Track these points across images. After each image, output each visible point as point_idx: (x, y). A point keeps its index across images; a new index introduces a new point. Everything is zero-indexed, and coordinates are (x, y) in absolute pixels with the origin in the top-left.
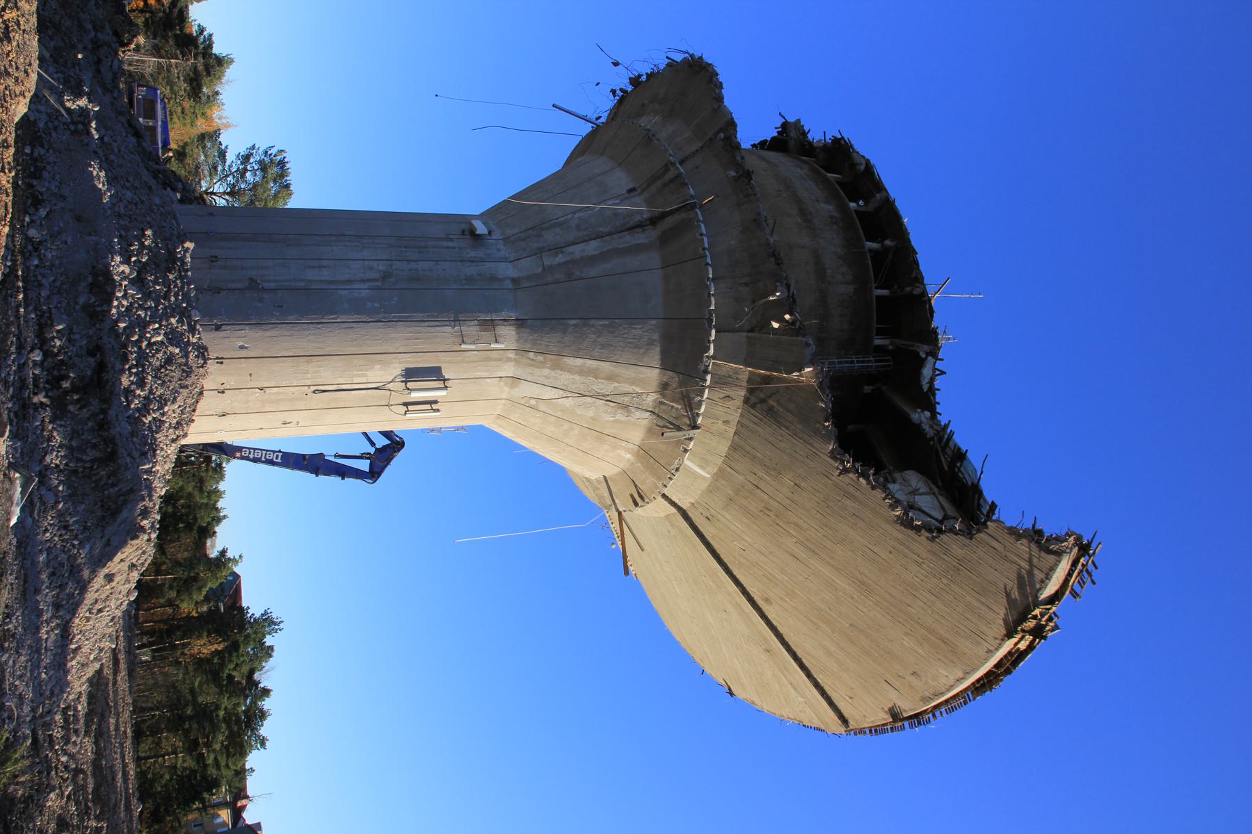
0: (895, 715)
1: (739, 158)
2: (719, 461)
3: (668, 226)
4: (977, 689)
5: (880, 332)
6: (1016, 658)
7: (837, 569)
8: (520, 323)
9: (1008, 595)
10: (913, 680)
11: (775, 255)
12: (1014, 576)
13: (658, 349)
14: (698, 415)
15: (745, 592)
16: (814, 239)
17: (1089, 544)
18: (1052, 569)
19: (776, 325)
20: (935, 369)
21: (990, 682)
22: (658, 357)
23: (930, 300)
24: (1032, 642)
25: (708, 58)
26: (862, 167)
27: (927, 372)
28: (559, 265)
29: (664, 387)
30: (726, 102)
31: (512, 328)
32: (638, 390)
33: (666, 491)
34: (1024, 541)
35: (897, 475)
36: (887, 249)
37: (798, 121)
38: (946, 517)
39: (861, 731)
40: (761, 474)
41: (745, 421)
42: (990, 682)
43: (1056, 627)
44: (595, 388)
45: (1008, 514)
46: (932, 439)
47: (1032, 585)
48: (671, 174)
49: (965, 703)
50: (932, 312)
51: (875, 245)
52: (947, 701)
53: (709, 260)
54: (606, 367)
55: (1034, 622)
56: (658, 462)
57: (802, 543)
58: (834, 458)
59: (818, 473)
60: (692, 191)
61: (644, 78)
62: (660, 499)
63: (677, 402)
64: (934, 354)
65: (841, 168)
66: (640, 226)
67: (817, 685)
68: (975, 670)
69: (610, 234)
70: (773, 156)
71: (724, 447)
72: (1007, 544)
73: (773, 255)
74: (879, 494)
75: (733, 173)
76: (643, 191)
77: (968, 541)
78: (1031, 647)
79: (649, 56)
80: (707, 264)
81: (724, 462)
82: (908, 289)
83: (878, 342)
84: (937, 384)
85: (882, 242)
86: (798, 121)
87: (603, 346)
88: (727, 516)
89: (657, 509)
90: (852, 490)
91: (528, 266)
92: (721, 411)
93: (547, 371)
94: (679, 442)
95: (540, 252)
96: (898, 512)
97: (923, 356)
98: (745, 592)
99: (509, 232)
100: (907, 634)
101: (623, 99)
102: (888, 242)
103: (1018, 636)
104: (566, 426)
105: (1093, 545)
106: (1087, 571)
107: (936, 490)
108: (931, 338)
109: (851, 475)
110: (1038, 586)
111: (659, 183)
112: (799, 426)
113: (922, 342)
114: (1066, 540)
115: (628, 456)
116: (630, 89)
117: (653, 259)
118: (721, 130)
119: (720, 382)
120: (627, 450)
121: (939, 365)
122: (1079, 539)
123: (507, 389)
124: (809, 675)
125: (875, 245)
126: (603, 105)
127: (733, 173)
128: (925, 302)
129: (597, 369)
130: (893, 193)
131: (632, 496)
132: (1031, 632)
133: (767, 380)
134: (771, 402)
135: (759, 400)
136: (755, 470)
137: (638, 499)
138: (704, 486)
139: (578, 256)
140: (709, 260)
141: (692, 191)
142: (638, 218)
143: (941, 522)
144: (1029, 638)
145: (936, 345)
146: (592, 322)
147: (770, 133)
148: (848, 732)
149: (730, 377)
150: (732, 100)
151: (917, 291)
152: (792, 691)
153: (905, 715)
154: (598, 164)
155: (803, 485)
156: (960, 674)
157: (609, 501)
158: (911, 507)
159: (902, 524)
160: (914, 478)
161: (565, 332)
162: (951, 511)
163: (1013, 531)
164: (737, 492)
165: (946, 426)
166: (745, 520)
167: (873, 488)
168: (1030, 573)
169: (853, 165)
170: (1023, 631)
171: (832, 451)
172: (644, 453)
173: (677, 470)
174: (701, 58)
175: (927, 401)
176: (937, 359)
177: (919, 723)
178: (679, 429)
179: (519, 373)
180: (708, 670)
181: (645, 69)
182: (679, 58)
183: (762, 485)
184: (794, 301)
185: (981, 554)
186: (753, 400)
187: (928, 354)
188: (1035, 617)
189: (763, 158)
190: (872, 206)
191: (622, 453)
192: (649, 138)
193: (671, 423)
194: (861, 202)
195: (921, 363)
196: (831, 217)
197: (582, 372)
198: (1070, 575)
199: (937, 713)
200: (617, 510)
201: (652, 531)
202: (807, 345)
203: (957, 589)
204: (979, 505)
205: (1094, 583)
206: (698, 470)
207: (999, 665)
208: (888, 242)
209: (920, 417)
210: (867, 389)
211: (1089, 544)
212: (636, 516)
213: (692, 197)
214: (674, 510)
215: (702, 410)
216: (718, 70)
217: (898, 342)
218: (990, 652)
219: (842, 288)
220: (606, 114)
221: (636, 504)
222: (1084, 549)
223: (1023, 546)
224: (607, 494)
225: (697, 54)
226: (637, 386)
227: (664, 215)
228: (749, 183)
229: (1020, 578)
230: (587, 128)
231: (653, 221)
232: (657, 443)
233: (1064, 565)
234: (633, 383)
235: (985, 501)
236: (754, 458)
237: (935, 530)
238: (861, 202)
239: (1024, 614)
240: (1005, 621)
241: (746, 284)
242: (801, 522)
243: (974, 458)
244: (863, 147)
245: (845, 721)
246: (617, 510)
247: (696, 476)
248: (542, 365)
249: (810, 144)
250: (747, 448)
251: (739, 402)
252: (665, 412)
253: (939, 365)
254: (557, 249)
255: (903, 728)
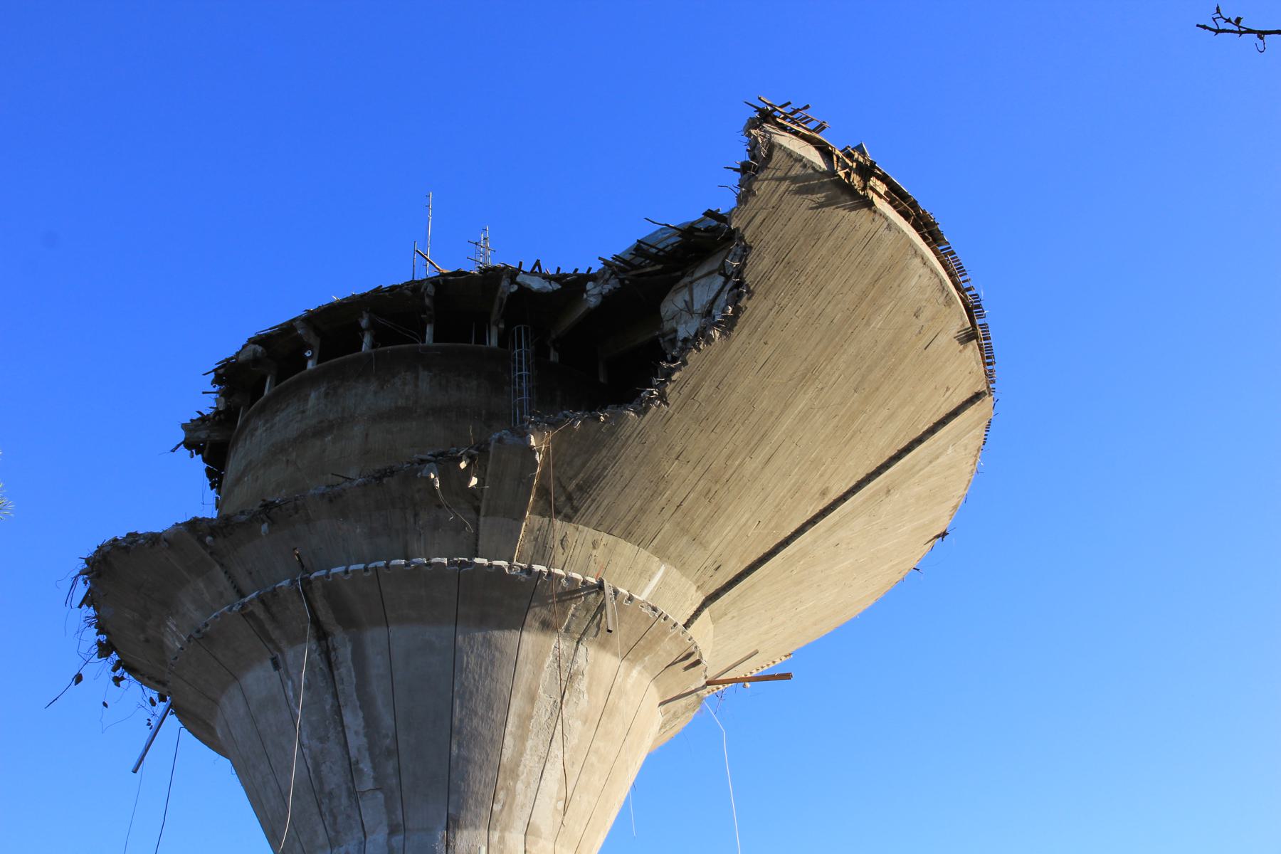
0: (968, 337)
1: (243, 518)
2: (644, 554)
3: (332, 617)
4: (935, 240)
5: (481, 339)
6: (897, 196)
7: (786, 406)
8: (453, 824)
9: (821, 205)
10: (923, 316)
11: (380, 476)
12: (798, 199)
13: (497, 633)
14: (584, 582)
15: (813, 521)
16: (361, 422)
17: (758, 110)
18: (790, 154)
19: (474, 481)
20: (532, 273)
21: (926, 225)
22: (507, 633)
23: (443, 275)
24: (878, 177)
25: (90, 549)
26: (259, 349)
27: (536, 284)
28: (374, 768)
29: (546, 626)
30: (157, 528)
31: (458, 836)
32: (550, 659)
33: (681, 624)
34: (755, 186)
35: (667, 326)
36: (373, 325)
37: (184, 426)
38: (722, 271)
39: (989, 375)
40: (663, 501)
41: (594, 521)
42: (926, 225)
43: (860, 149)
44: (544, 719)
45: (725, 203)
46: (622, 281)
47: (808, 178)
48: (260, 612)
49: (952, 253)
50: (458, 273)
51: (367, 340)
52: (951, 275)
53: (382, 564)
54: (517, 704)
55: (853, 176)
56: (645, 634)
57: (752, 451)
58: (646, 411)
59: (666, 432)
60: (285, 583)
61: (103, 638)
62: (690, 631)
63: (567, 609)
64: (513, 274)
65: (258, 378)
66: (327, 655)
67: (932, 430)
68: (911, 244)
69: (335, 696)
70: (234, 465)
71: (627, 548)
72: (758, 206)
73: (380, 479)
74: (693, 356)
75: (265, 527)
76: (279, 650)
77: (754, 252)
78: (884, 179)
79: (74, 631)
80: (387, 566)
81: (646, 548)
82: (427, 301)
83: (494, 342)
84: (552, 271)
85: (362, 330)
86: (184, 426)
87: (490, 707)
88: (715, 544)
89: (704, 634)
90: (686, 390)
91: (373, 811)
92: (580, 552)
93: (520, 786)
94: (620, 606)
95: (354, 795)
96: (716, 334)
97: (515, 288)
98: (813, 521)
99: (322, 838)
100: (868, 324)
101: (127, 666)
102: (364, 323)
103: (871, 194)
104: (593, 758)
105: (762, 106)
106: (792, 113)
107: (687, 280)
108: (492, 276)
109: (668, 390)
110: (810, 171)
111: (269, 626)
112: (604, 452)
113: (499, 284)
114: (756, 138)
115: (635, 673)
116: (115, 657)
117: (374, 637)
118: (201, 540)
119: (542, 551)
120: (627, 675)
121: (527, 267)
122: (753, 124)
123: (542, 842)
124: (919, 441)
125: (367, 340)
126: (134, 692)
127: (265, 527)
128: (445, 281)
129: (519, 716)
130: (298, 312)
131: (686, 668)
132: (865, 179)
133: (543, 492)
134: (571, 487)
135: (568, 500)
136: (658, 509)
137: (691, 660)
138: (675, 573)
139: (363, 741)
140: (382, 564)
141: (285, 583)
142: (316, 656)
143: (728, 278)
144: (873, 181)
145: (503, 269)
146: (456, 722)
147: (197, 465)
148: (991, 391)
149: (536, 539)
150: (159, 517)
151: (431, 290)
152: (940, 460)
153: (969, 325)
154: (231, 708)
155: (678, 449)
156: (917, 261)
157: (693, 698)
158: (708, 313)
159: (731, 329)
160: (673, 304)
161: (467, 760)
162: (714, 263)
163: (742, 199)
164: (685, 531)
165: (606, 263)
166: (721, 521)
167: (685, 363)
168: (794, 180)
169: (256, 360)
170: (864, 189)
171: (638, 413)
172: (631, 653)
173: (654, 609)
174: (87, 561)
175: (573, 285)
176: (519, 269)
177: (979, 307)
178: (602, 607)
179: (520, 825)
180: (914, 564)
181: (92, 636)
182: (82, 590)
183: (677, 500)
184: (442, 454)
185: (769, 236)
186: (567, 510)
187: (513, 281)
188: (848, 175)
189: (238, 480)
190: (314, 340)
191: (630, 681)
192: (202, 638)
193: (594, 617)
194: (308, 354)
195: (524, 290)
196: (327, 394)
197: (522, 739)
198: (796, 133)
199: (965, 285)
200: (704, 687)
201: (736, 639)
202: (500, 440)
203: (812, 265)
204: (707, 230)
205: (807, 107)
206: (654, 582)
207: (906, 215)
208: (364, 323)
209: (593, 295)
210: (554, 357)
211: (758, 110)
212: (713, 664)
213: (293, 582)
214: (706, 612)
215: (579, 577)
216: (109, 537)
217: (495, 316)
218: (890, 226)
219: (421, 387)
220: (147, 690)
221: (698, 662)
222: (766, 116)
223: (762, 187)
224: (683, 702)
225: (82, 565)
226: (543, 661)
227: (316, 622)
228: (278, 506)
229: (800, 192)
230: (173, 721)
231: (322, 635)
232: (618, 637)
233: (786, 140)
234: (539, 668)
235: (701, 221)
236: (642, 510)
237: (738, 289)
238: (308, 354)
239: (845, 184)
240: (852, 209)
241: (416, 515)
242: (726, 452)
243: (644, 231)
244: (230, 345)
245: (976, 397)
246: (704, 687)
247: (663, 583)
248: (511, 793)
249: (218, 412)
250: (629, 518)
251: (569, 528)
252: (579, 625)
253: (527, 267)
254: (352, 769)
255: (984, 326)
